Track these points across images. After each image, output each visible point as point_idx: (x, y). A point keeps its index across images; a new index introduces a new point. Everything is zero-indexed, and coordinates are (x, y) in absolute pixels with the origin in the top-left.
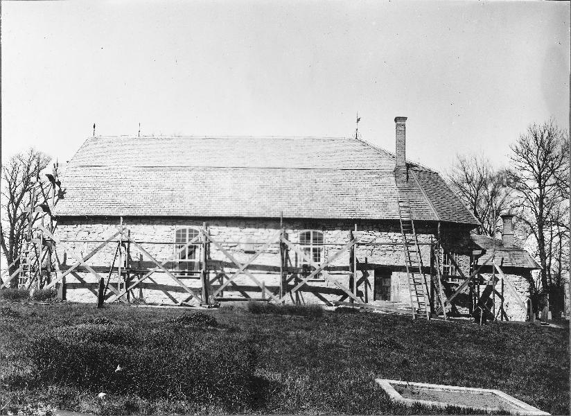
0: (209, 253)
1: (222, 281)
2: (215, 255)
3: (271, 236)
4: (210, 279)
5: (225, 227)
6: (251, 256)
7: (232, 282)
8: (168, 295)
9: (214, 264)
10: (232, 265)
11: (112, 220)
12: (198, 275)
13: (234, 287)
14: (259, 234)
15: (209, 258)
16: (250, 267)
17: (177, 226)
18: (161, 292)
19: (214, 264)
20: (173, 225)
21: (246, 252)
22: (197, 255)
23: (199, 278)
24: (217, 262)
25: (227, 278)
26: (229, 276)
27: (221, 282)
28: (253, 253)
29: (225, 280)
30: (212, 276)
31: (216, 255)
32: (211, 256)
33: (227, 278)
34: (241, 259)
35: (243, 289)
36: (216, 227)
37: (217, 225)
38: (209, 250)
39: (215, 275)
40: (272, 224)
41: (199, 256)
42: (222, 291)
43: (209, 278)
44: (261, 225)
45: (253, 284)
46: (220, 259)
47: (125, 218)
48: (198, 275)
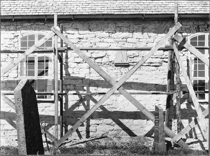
0: (67, 67)
1: (88, 105)
2: (75, 71)
3: (156, 41)
4: (70, 104)
5: (88, 32)
6: (123, 70)
7: (102, 107)
8: (121, 125)
9: (73, 82)
10: (107, 84)
11: (44, 21)
12: (52, 98)
13: (104, 114)
14: (134, 40)
15: (68, 74)
16: (127, 85)
17: (23, 31)
18: (110, 121)
19: (73, 82)
20: (16, 30)
21: (117, 65)
22: (50, 71)
23: (53, 102)
24: (76, 79)
25: (95, 101)
26: (97, 98)
27: (87, 107)
28: (127, 66)
29: (92, 103)
30: (72, 99)
31: (78, 70)
32: (70, 71)
33: (95, 101)
34: (117, 76)
35: (117, 117)
36: (76, 32)
37: (77, 29)
38: (67, 63)
39: (77, 98)
40: (152, 26)
41: (53, 74)
42: (88, 120)
43: (67, 101)
44: (136, 27)
45: (132, 108)
46: (81, 76)
47: (183, 18)
48: (52, 98)
